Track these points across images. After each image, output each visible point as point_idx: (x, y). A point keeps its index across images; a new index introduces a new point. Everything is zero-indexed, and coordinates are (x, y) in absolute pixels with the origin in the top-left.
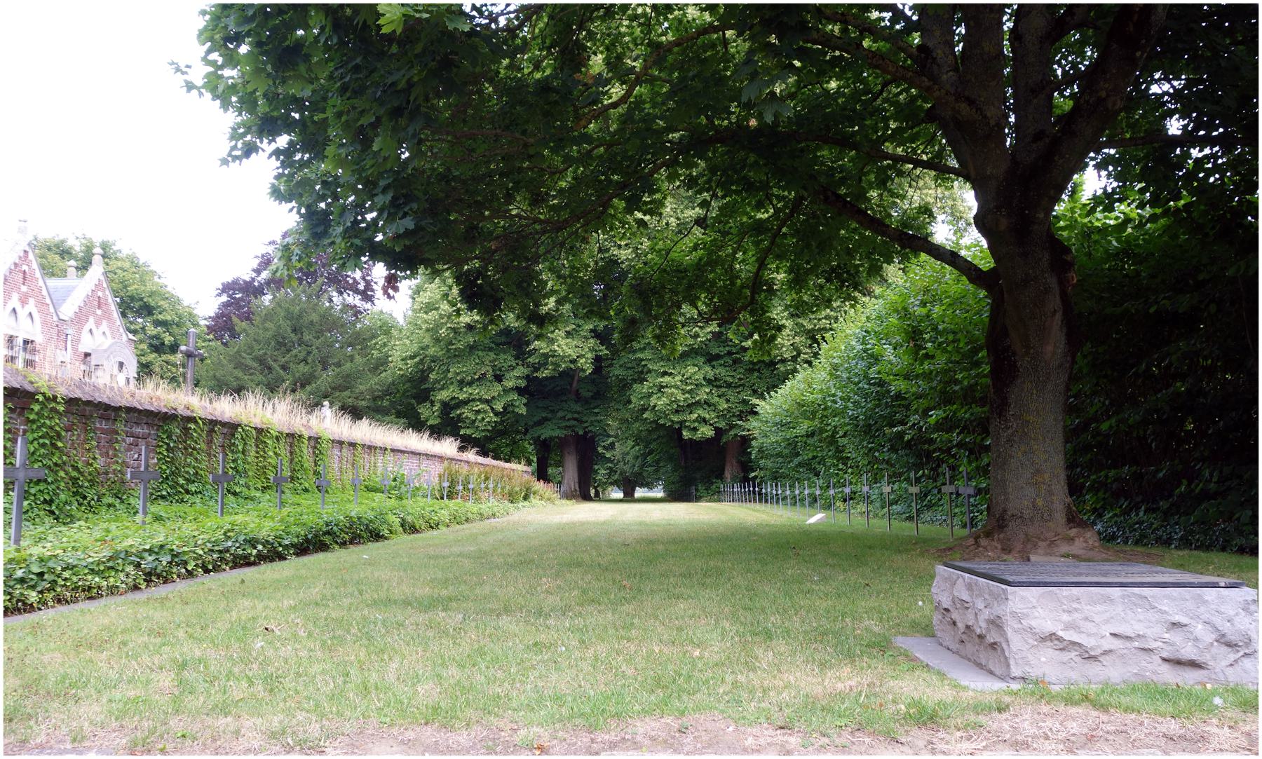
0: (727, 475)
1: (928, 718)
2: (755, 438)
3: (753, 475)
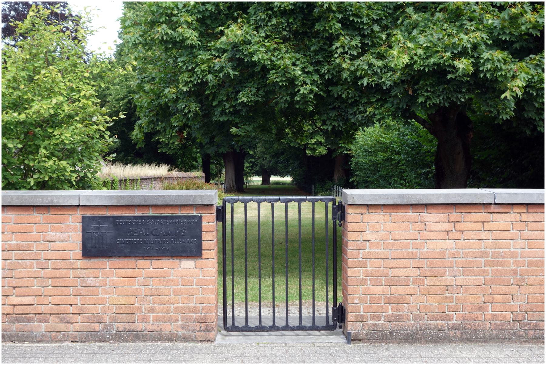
0: (336, 178)
1: (284, 335)
2: (353, 156)
3: (351, 180)
